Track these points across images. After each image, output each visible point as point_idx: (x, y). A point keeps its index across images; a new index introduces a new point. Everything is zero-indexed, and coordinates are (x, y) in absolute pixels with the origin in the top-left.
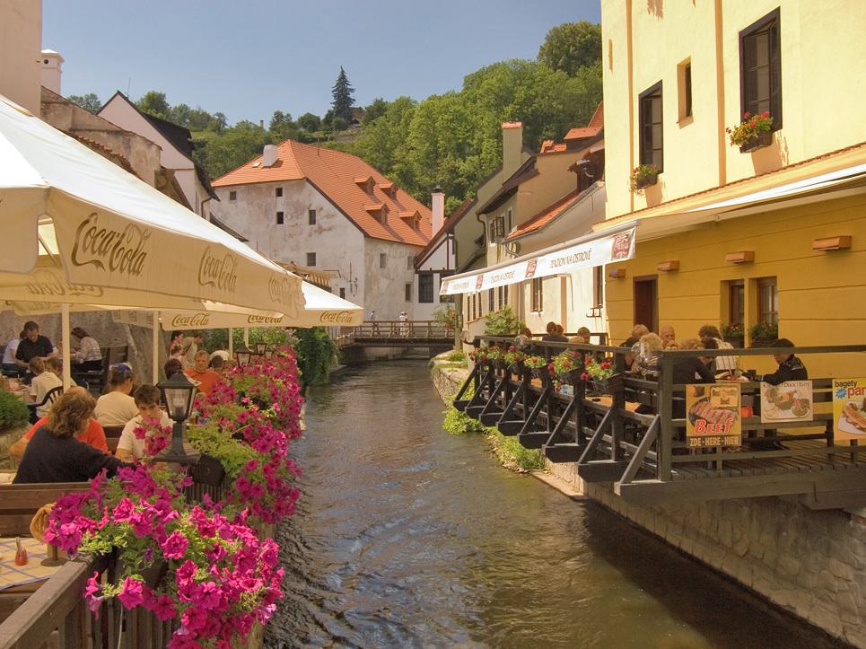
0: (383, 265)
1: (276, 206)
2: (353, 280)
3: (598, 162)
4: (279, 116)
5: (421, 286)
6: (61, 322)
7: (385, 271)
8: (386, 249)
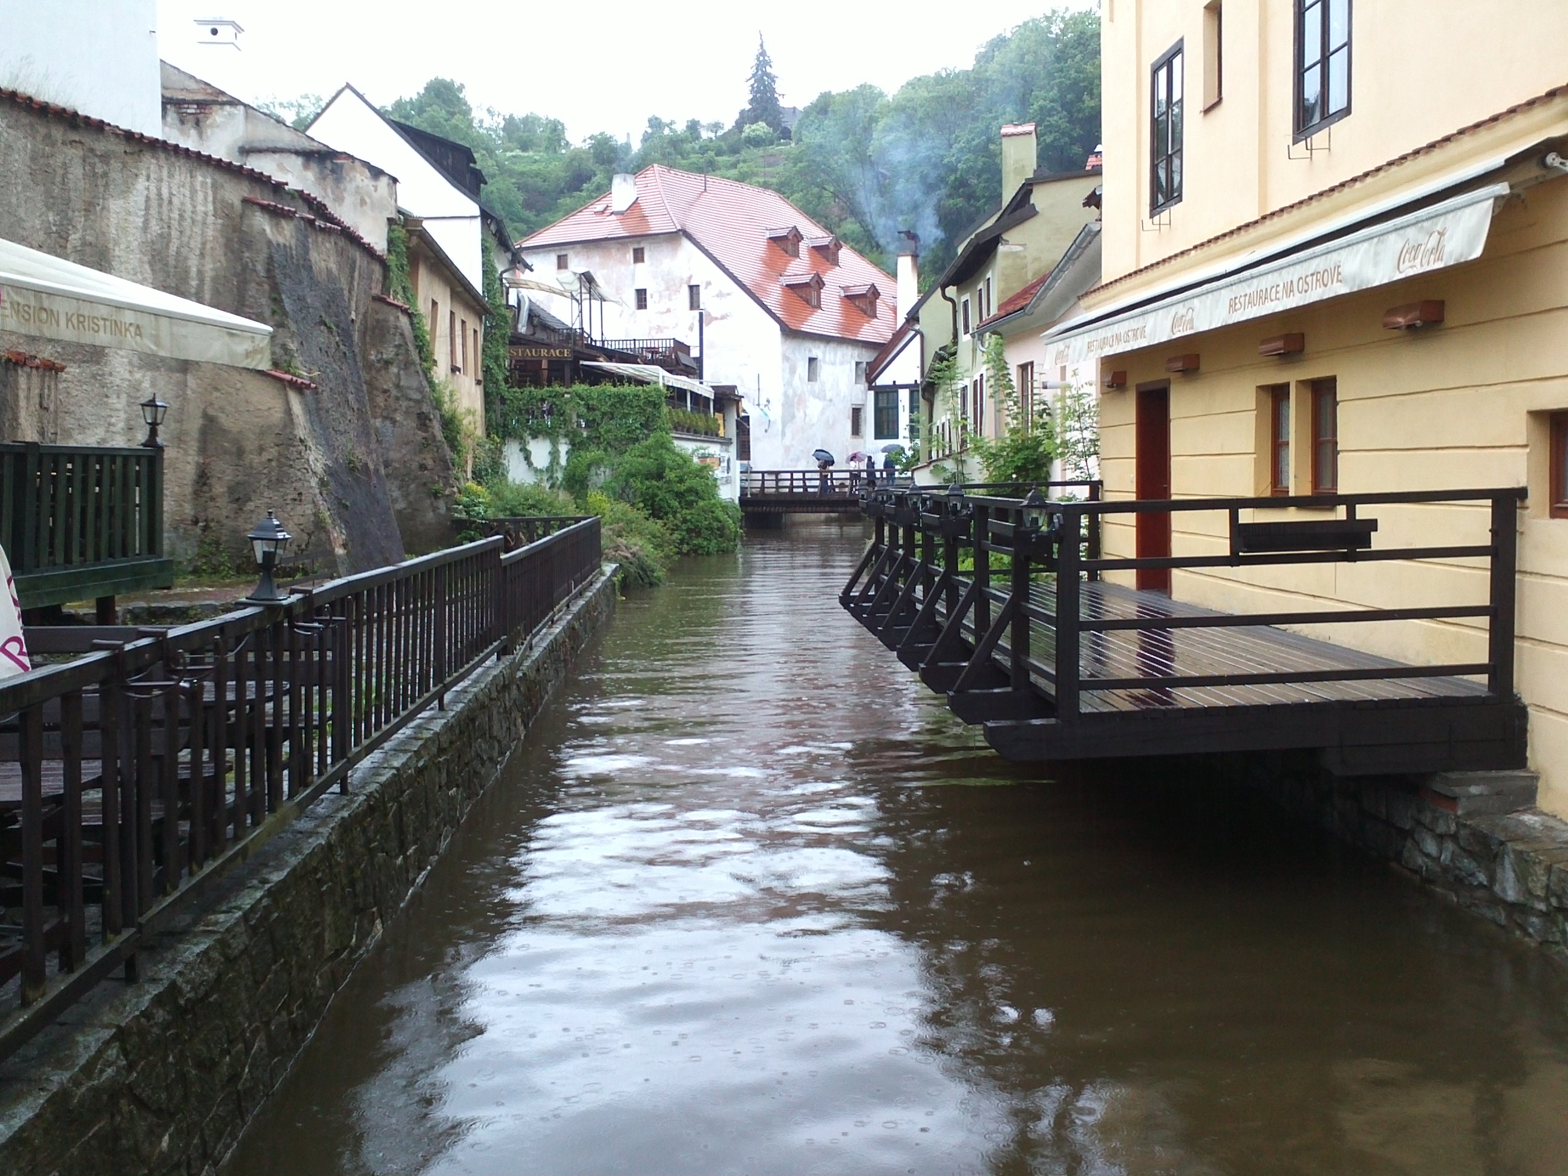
0: (812, 375)
1: (633, 279)
2: (763, 402)
3: (415, 240)
4: (656, 123)
5: (878, 411)
6: (1382, 214)
7: (816, 386)
8: (817, 350)
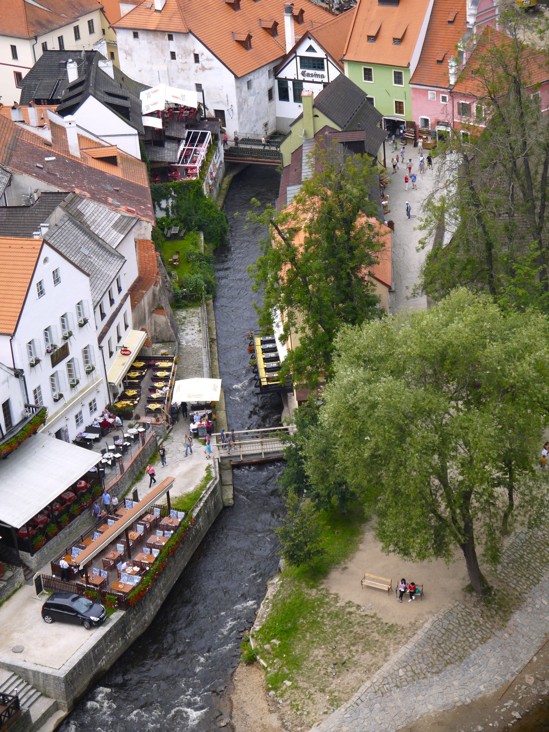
7: (252, 91)
